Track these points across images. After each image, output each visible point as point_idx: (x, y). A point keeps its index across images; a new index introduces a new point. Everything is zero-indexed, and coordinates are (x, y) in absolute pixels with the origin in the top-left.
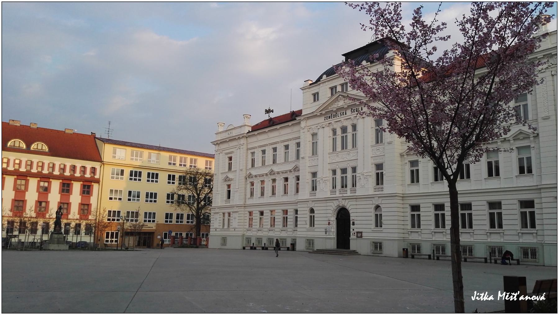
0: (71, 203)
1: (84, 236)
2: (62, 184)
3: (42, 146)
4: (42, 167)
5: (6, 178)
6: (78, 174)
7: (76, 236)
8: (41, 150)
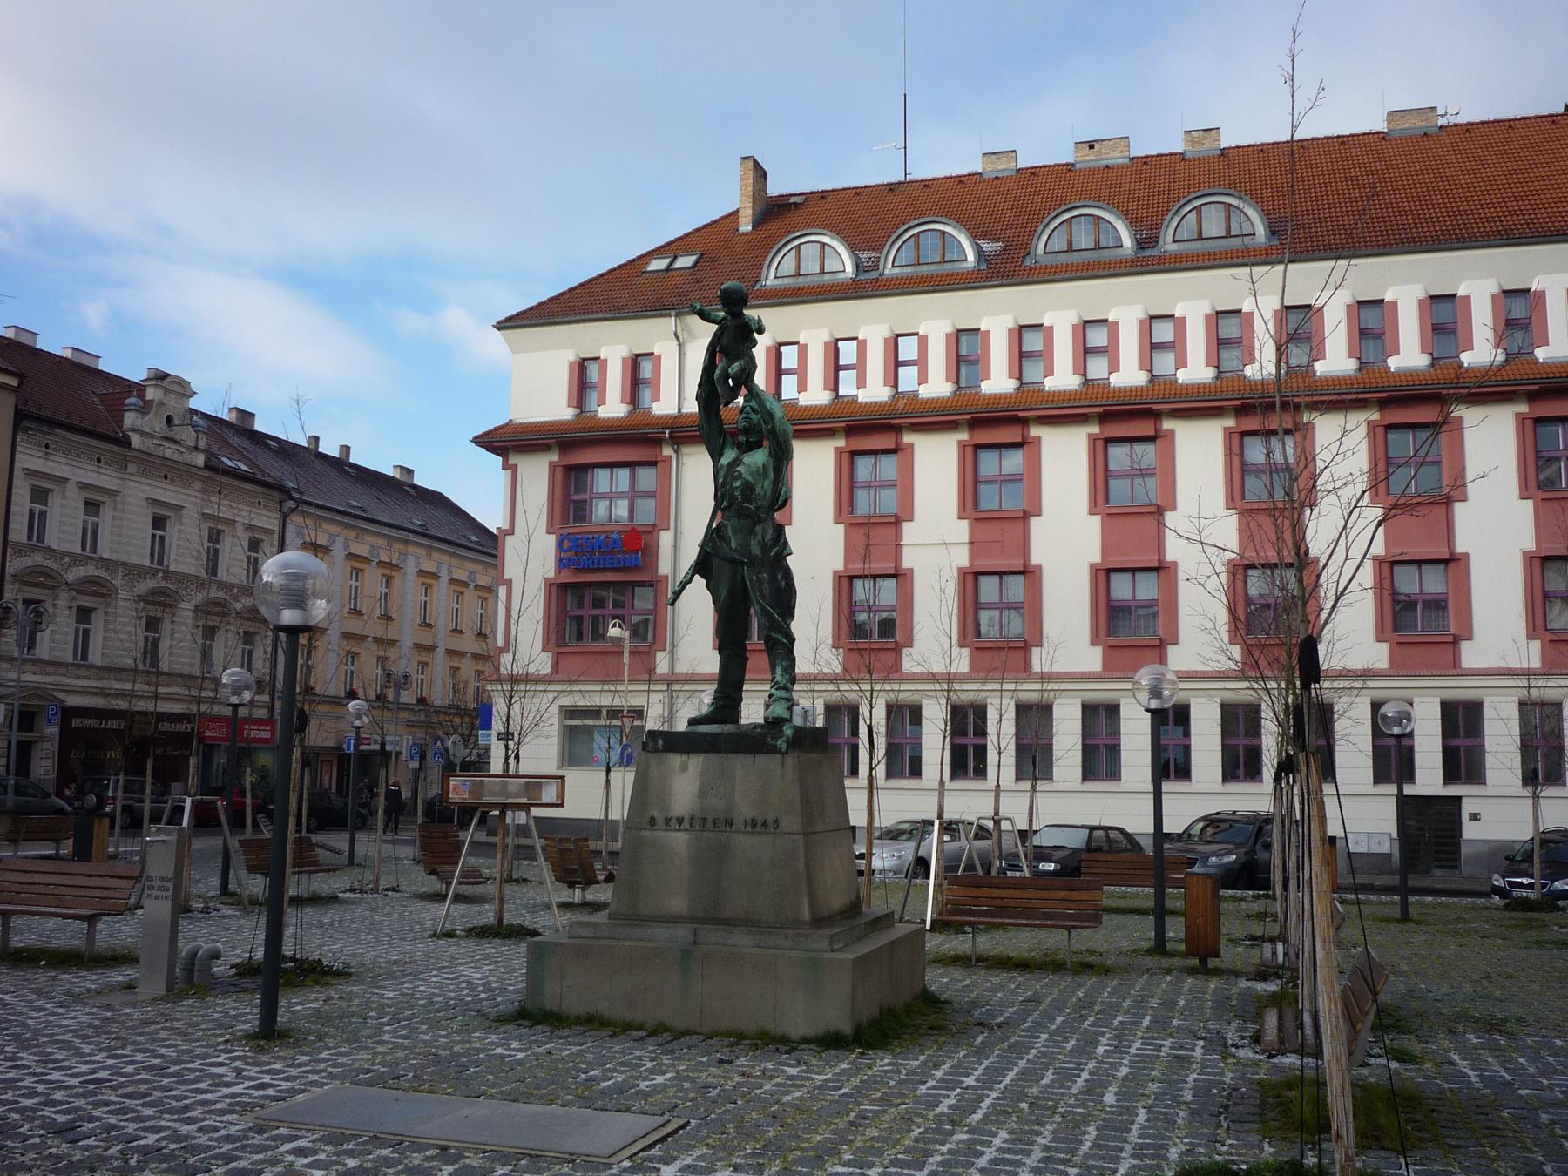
0: (911, 570)
1: (1077, 784)
2: (559, 473)
3: (1228, 219)
4: (1243, 344)
5: (916, 448)
6: (1481, 352)
7: (1027, 785)
8: (1223, 242)
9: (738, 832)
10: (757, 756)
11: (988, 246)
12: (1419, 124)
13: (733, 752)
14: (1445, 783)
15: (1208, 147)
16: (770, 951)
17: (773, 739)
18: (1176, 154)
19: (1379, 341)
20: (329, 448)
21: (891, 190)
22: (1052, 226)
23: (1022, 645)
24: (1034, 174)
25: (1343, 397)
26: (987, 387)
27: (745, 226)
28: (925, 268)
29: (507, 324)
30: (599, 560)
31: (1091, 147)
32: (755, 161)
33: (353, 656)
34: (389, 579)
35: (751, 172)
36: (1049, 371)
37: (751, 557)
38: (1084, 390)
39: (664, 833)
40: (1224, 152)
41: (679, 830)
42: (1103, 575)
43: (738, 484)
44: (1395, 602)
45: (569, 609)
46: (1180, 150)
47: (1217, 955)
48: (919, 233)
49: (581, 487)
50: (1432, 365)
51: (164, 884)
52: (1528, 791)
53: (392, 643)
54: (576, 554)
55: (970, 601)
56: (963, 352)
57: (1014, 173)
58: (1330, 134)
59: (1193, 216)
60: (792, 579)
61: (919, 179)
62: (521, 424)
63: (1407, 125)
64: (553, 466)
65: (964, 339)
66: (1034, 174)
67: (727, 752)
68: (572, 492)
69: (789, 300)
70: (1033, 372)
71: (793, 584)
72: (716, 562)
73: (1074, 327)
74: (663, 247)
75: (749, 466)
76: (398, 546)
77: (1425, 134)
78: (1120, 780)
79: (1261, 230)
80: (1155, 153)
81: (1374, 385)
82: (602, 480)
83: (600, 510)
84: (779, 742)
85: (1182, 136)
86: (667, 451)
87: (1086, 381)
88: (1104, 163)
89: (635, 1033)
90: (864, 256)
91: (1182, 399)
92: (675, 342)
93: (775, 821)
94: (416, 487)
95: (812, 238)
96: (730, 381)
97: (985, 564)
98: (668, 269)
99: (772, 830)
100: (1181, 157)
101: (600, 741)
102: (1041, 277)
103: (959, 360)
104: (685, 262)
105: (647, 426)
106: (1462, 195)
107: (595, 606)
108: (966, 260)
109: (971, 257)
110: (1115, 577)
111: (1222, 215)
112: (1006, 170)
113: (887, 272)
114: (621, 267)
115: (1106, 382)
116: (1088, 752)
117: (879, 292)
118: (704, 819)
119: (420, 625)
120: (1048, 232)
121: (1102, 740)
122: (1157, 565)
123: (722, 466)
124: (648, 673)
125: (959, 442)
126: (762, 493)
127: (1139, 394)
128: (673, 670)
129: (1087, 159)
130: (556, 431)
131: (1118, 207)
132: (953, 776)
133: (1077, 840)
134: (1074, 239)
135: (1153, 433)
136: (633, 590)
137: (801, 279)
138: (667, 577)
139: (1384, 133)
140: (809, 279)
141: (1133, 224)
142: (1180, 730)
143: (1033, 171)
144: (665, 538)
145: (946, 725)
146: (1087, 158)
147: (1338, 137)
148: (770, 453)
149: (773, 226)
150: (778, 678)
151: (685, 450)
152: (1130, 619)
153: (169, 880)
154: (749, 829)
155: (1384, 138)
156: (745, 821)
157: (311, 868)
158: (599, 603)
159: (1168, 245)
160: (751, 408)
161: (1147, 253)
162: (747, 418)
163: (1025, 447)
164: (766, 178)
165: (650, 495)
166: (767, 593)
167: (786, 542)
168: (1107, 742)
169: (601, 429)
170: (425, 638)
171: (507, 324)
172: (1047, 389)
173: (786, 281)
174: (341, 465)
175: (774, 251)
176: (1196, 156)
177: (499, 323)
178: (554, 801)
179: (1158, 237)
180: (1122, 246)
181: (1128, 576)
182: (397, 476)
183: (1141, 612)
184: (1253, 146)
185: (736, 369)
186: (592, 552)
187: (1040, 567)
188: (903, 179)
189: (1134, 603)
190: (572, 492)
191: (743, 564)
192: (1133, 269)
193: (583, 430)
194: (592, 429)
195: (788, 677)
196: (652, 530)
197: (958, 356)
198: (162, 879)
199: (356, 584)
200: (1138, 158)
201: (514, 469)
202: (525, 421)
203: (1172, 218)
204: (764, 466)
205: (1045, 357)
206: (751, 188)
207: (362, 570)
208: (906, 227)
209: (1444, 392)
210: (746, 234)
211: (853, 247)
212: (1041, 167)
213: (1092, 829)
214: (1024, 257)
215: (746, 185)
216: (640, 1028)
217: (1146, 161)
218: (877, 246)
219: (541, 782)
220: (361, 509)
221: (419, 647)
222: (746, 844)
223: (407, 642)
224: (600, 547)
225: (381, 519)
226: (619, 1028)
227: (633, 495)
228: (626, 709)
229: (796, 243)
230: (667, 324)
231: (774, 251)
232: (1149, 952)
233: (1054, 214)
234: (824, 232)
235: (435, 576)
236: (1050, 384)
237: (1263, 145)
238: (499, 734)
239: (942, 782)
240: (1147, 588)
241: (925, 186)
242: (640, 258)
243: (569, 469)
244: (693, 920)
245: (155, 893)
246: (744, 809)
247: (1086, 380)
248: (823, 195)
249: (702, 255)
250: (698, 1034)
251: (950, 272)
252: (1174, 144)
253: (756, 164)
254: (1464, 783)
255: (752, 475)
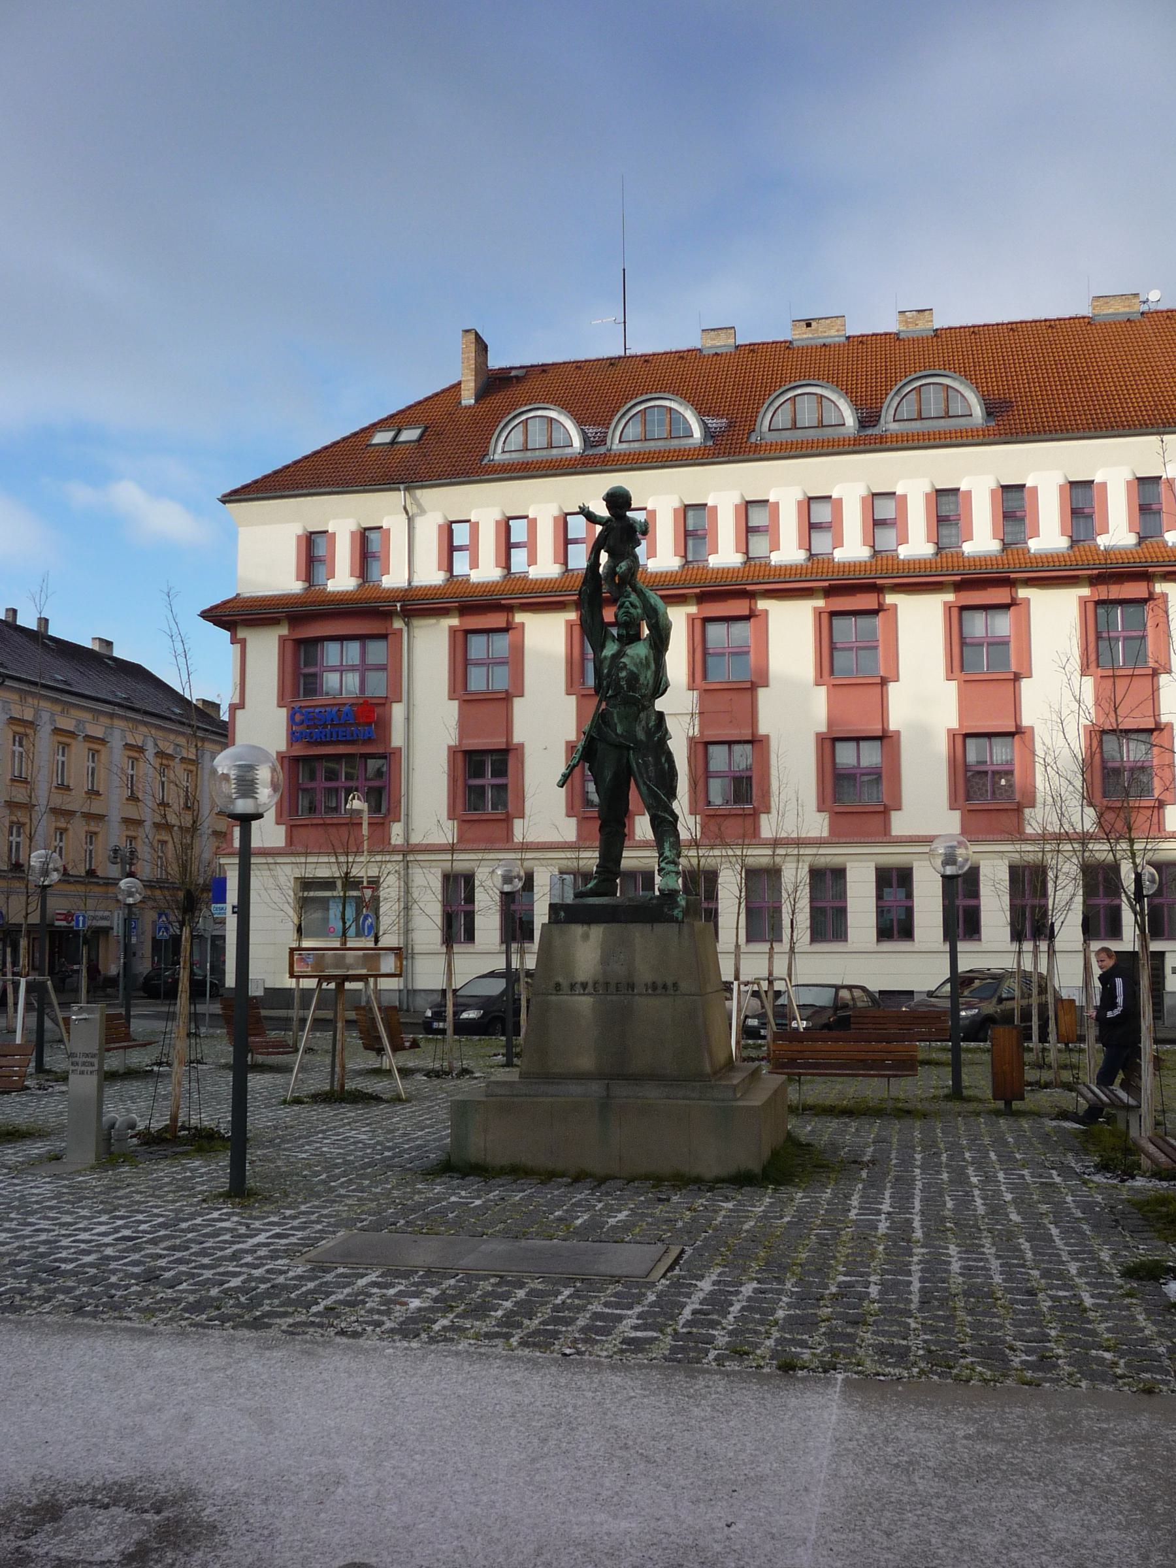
2: (289, 646)
9: (640, 995)
10: (655, 925)
11: (713, 423)
12: (1122, 310)
13: (632, 922)
14: (878, 940)
15: (923, 326)
16: (680, 1102)
17: (669, 909)
18: (890, 334)
19: (1090, 520)
20: (28, 620)
21: (611, 364)
22: (777, 404)
23: (752, 812)
24: (753, 351)
25: (1079, 573)
26: (714, 561)
27: (468, 399)
28: (651, 444)
29: (232, 498)
30: (331, 734)
31: (809, 325)
32: (477, 334)
33: (62, 832)
34: (94, 753)
35: (473, 345)
36: (775, 546)
37: (638, 742)
38: (810, 564)
39: (569, 998)
40: (937, 333)
41: (584, 994)
42: (829, 742)
43: (623, 674)
44: (1104, 768)
45: (300, 781)
46: (895, 330)
47: (1022, 1098)
48: (645, 409)
49: (311, 660)
50: (1139, 544)
51: (89, 1060)
52: (1015, 947)
53: (100, 818)
54: (308, 727)
55: (700, 771)
56: (690, 528)
57: (733, 350)
58: (1037, 318)
59: (913, 395)
60: (674, 762)
61: (639, 354)
62: (248, 598)
63: (1111, 311)
64: (283, 640)
65: (690, 514)
66: (753, 351)
67: (626, 922)
68: (302, 666)
69: (519, 474)
70: (759, 546)
71: (674, 766)
72: (600, 746)
73: (799, 503)
74: (386, 419)
75: (632, 658)
76: (104, 720)
77: (1128, 320)
78: (847, 941)
79: (978, 411)
80: (871, 333)
81: (1092, 562)
82: (332, 653)
83: (331, 680)
84: (676, 912)
85: (896, 316)
86: (398, 624)
87: (811, 556)
88: (822, 341)
89: (560, 1180)
90: (591, 431)
91: (905, 574)
92: (405, 516)
93: (675, 985)
94: (115, 660)
95: (539, 413)
96: (617, 578)
97: (713, 734)
98: (393, 442)
99: (672, 992)
100: (896, 337)
101: (334, 911)
102: (767, 454)
103: (687, 534)
104: (410, 435)
105: (378, 599)
106: (1165, 380)
107: (328, 779)
108: (692, 436)
109: (697, 433)
110: (839, 746)
111: (942, 395)
112: (725, 346)
113: (614, 447)
114: (344, 439)
115: (830, 556)
116: (816, 913)
117: (607, 468)
118: (607, 984)
119: (127, 799)
120: (772, 409)
121: (828, 903)
122: (880, 734)
123: (605, 657)
124: (381, 844)
125: (688, 615)
126: (645, 683)
127: (852, 569)
128: (408, 842)
129: (801, 336)
130: (285, 605)
131: (837, 386)
132: (749, 940)
133: (824, 998)
134: (798, 417)
135: (877, 607)
136: (366, 762)
137: (529, 454)
138: (401, 748)
139: (1089, 317)
140: (537, 453)
141: (856, 404)
142: (901, 894)
143: (752, 348)
144: (398, 711)
145: (741, 892)
146: (805, 336)
147: (1046, 320)
148: (650, 645)
149: (497, 399)
150: (667, 853)
151: (416, 622)
152: (855, 786)
153: (94, 1056)
154: (650, 991)
155: (1089, 323)
156: (646, 985)
157: (125, 1044)
158: (332, 775)
159: (888, 424)
160: (631, 603)
161: (870, 432)
162: (628, 612)
163: (752, 620)
164: (486, 351)
165: (382, 668)
166: (652, 774)
167: (666, 729)
168: (831, 904)
169: (331, 602)
170: (132, 812)
171: (232, 498)
172: (773, 563)
173: (514, 455)
174: (39, 638)
175: (502, 425)
176: (910, 335)
177: (224, 496)
178: (393, 971)
179: (880, 416)
180: (844, 425)
181: (853, 745)
182: (96, 648)
183: (865, 778)
184: (965, 327)
185: (624, 568)
186: (325, 725)
187: (767, 737)
188: (623, 354)
189: (859, 771)
190: (302, 666)
191: (629, 748)
192: (857, 448)
193: (313, 603)
194: (323, 603)
195: (675, 852)
196: (385, 703)
197: (686, 531)
198: (87, 1055)
199: (63, 759)
200: (854, 337)
201: (243, 643)
202: (253, 594)
203: (892, 399)
204: (646, 657)
205: (771, 531)
206: (473, 362)
207: (68, 745)
208: (632, 403)
209: (1150, 570)
210: (469, 407)
211: (580, 422)
212: (759, 344)
213: (838, 988)
214: (749, 434)
215: (468, 358)
216: (563, 1175)
217: (862, 340)
218: (604, 421)
219: (345, 954)
220: (65, 682)
221: (127, 821)
222: (647, 1005)
223: (115, 816)
224: (332, 720)
225: (87, 693)
226: (548, 1176)
227: (364, 668)
228: (365, 880)
229: (524, 417)
230: (397, 498)
231: (502, 425)
232: (947, 1098)
233: (781, 391)
234: (552, 407)
235: (141, 750)
236: (776, 558)
237: (974, 327)
238: (234, 907)
239: (737, 946)
240: (871, 756)
241: (646, 361)
242: (363, 430)
243: (299, 642)
244: (599, 1076)
245: (80, 1068)
246: (644, 973)
247: (811, 555)
248: (544, 369)
249: (426, 428)
250: (619, 1178)
251: (677, 448)
252: (889, 324)
253: (478, 339)
254: (1166, 939)
255: (636, 665)
